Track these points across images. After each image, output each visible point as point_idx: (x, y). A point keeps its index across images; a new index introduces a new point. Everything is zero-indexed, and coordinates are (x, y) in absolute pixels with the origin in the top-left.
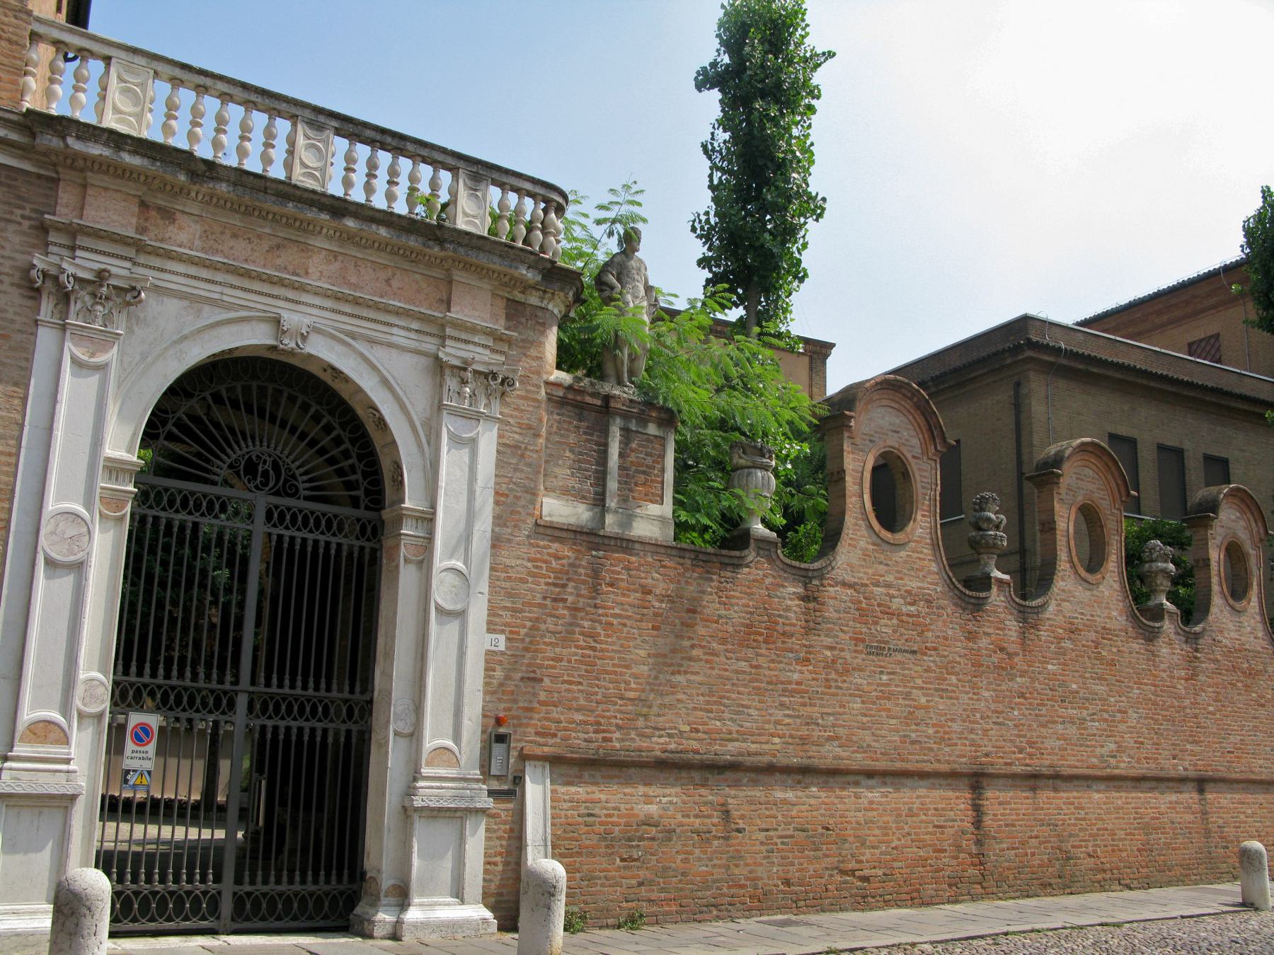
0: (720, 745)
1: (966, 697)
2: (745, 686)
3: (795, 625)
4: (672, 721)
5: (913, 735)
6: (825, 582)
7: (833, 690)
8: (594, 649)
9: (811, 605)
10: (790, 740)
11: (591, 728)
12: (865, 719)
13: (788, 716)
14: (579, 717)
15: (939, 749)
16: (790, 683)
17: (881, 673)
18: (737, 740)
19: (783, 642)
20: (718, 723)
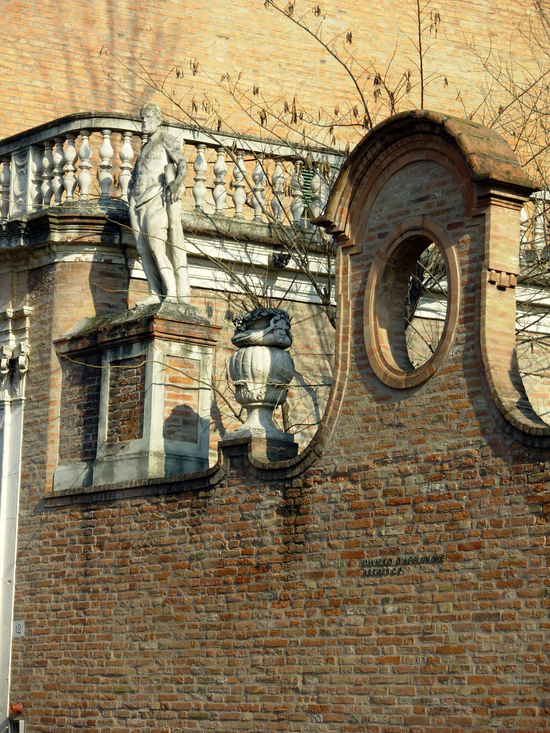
0: (190, 725)
1: (534, 625)
2: (215, 645)
3: (270, 553)
4: (145, 698)
5: (436, 699)
6: (311, 480)
7: (318, 638)
8: (84, 622)
9: (292, 519)
10: (263, 716)
11: (79, 712)
12: (360, 677)
13: (262, 681)
14: (71, 700)
15: (482, 722)
16: (264, 634)
17: (385, 601)
18: (206, 718)
19: (258, 578)
20: (187, 696)
